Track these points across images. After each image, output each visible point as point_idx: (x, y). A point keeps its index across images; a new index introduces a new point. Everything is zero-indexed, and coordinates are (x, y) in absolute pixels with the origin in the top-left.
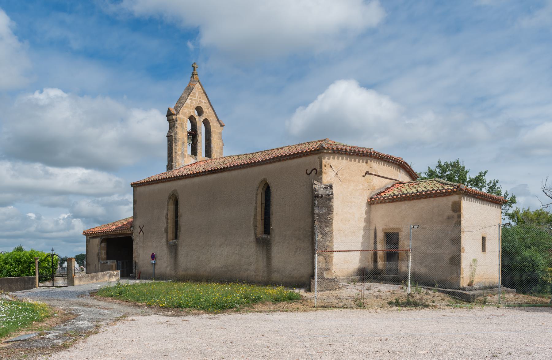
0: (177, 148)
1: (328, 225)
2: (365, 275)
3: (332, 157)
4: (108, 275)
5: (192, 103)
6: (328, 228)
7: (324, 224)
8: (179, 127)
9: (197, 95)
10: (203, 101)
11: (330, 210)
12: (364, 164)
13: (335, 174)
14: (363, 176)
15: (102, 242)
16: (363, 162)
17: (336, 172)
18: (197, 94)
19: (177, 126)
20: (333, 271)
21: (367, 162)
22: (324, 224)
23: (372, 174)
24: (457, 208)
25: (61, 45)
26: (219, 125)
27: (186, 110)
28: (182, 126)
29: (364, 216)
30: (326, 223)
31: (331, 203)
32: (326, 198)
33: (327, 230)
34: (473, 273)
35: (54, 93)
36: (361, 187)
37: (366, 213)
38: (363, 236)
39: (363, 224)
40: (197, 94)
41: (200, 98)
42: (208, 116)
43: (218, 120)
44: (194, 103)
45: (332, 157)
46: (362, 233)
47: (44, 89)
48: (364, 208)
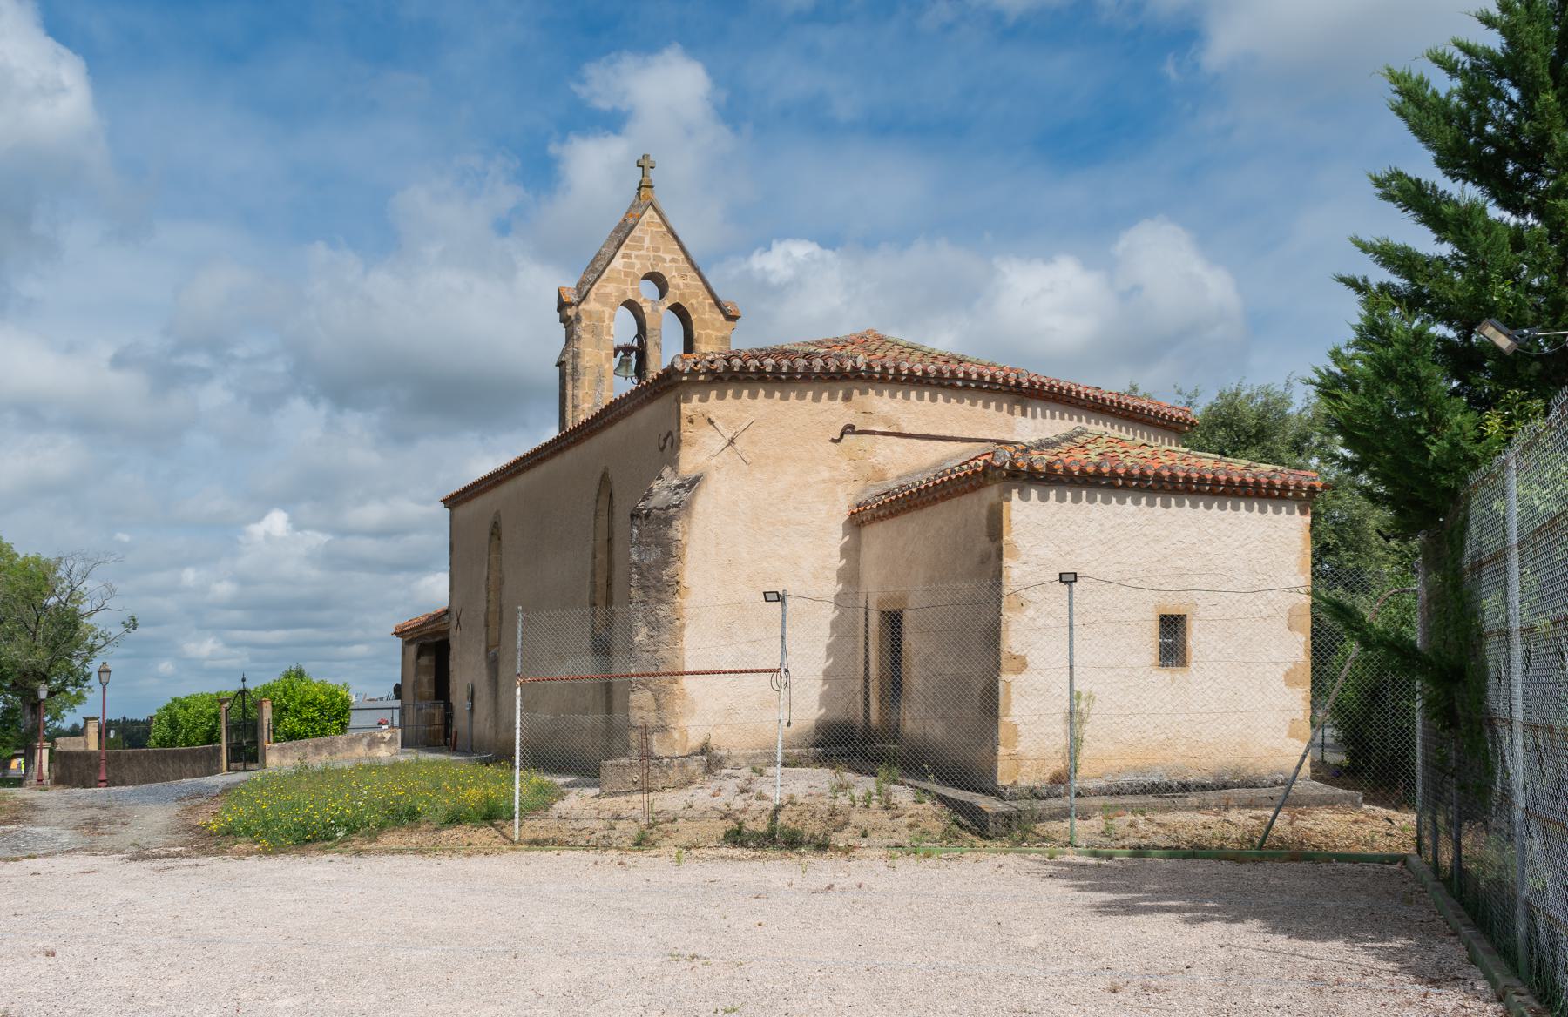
0: (580, 393)
1: (663, 596)
2: (839, 744)
3: (713, 393)
4: (365, 741)
5: (632, 266)
6: (665, 607)
7: (653, 594)
8: (585, 336)
9: (647, 242)
10: (668, 257)
11: (668, 552)
12: (838, 403)
13: (725, 442)
14: (833, 441)
15: (419, 654)
16: (832, 397)
17: (730, 435)
18: (647, 239)
19: (581, 333)
20: (676, 735)
21: (847, 398)
22: (653, 594)
23: (873, 433)
24: (995, 527)
25: (814, 120)
26: (722, 318)
27: (610, 288)
28: (595, 332)
29: (837, 562)
30: (658, 591)
31: (672, 533)
32: (658, 517)
33: (663, 611)
34: (1075, 745)
35: (801, 250)
36: (826, 475)
37: (844, 552)
38: (834, 625)
39: (833, 587)
40: (647, 239)
41: (656, 250)
42: (682, 295)
43: (718, 304)
44: (638, 264)
45: (713, 393)
46: (829, 613)
47: (774, 243)
48: (836, 537)
